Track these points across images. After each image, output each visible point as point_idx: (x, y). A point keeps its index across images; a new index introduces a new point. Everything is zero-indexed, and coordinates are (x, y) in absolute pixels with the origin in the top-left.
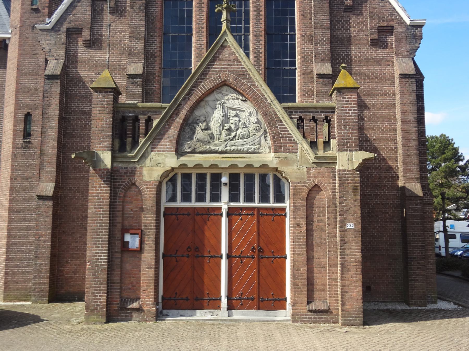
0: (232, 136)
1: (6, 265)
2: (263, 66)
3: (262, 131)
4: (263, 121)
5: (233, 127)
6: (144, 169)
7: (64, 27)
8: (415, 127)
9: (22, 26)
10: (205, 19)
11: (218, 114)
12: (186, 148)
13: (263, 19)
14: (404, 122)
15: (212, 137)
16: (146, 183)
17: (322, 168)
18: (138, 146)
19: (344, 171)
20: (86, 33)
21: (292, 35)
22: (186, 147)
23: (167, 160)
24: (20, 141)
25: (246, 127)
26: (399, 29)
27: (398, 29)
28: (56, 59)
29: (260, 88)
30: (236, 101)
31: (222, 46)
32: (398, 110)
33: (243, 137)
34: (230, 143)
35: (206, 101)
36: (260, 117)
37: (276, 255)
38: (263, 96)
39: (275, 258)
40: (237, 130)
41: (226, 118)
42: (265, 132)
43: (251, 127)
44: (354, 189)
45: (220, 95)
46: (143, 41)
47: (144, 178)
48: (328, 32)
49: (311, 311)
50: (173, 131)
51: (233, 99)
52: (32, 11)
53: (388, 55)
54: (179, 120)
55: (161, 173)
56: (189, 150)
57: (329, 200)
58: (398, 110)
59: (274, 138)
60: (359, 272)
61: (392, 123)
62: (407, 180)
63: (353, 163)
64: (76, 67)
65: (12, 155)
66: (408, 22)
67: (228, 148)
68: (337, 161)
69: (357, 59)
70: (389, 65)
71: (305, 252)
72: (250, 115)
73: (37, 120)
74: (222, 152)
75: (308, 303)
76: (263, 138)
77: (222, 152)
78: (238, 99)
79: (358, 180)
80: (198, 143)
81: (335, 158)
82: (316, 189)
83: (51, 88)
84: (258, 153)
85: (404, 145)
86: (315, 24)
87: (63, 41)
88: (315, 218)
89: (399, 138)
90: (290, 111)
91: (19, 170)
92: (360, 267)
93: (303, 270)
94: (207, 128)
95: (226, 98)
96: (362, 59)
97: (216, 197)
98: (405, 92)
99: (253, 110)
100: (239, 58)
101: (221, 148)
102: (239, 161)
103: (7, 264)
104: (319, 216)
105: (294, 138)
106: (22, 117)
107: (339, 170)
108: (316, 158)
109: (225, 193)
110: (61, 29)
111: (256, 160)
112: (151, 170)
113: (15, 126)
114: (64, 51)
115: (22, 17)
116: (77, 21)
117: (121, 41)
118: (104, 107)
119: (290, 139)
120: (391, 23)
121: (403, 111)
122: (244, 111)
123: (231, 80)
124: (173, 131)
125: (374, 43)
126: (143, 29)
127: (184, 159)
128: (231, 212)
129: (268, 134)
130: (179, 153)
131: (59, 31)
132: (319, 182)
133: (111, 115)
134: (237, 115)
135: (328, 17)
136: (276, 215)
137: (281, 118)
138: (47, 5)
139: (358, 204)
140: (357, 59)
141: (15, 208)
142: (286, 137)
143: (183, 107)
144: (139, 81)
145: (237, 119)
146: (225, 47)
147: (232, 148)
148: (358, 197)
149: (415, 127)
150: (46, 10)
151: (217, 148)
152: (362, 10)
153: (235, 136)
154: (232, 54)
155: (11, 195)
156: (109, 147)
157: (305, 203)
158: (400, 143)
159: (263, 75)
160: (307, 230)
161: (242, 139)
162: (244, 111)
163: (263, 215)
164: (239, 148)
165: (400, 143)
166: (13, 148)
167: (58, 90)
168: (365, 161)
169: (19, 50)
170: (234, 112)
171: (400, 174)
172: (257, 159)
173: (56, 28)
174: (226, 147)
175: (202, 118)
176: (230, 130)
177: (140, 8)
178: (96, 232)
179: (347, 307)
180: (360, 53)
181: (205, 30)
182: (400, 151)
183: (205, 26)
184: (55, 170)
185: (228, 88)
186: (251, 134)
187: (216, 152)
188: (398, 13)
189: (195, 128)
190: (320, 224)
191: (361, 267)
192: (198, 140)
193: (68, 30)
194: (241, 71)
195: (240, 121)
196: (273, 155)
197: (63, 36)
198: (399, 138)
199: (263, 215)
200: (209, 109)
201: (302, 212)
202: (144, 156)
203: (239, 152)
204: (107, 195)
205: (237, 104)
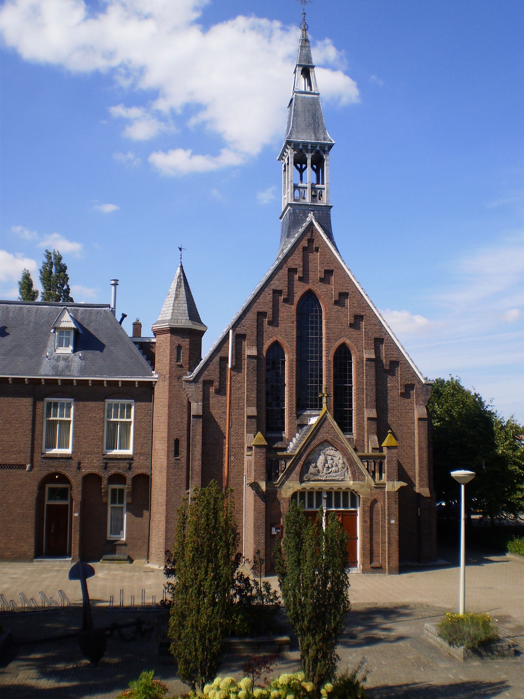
0: (330, 471)
1: (165, 543)
2: (332, 409)
3: (346, 468)
4: (346, 462)
5: (330, 466)
6: (282, 491)
7: (201, 380)
8: (426, 452)
9: (170, 377)
10: (295, 375)
11: (322, 458)
12: (305, 478)
13: (332, 377)
14: (420, 449)
15: (319, 471)
16: (284, 498)
17: (378, 490)
18: (278, 477)
19: (390, 492)
20: (216, 384)
21: (350, 386)
22: (305, 477)
23: (295, 486)
24: (173, 459)
25: (337, 466)
26: (419, 387)
27: (417, 386)
28: (196, 402)
29: (345, 444)
30: (332, 451)
31: (324, 419)
32: (416, 440)
33: (336, 472)
34: (328, 475)
35: (315, 451)
36: (345, 460)
37: (352, 538)
38: (347, 449)
39: (352, 539)
40: (332, 467)
41: (326, 461)
42: (348, 469)
43: (340, 466)
44: (395, 502)
45: (323, 447)
46: (255, 391)
47: (282, 496)
48: (374, 388)
49: (372, 568)
50: (298, 468)
51: (330, 450)
52: (177, 366)
53: (411, 403)
54: (301, 462)
55: (292, 493)
56: (306, 480)
57: (382, 508)
58: (416, 440)
59: (353, 473)
60: (397, 546)
61: (413, 448)
62: (421, 486)
63: (395, 488)
64: (209, 407)
65: (167, 468)
66: (424, 381)
67: (328, 478)
68: (386, 486)
69: (392, 405)
70: (411, 409)
71: (369, 536)
72: (339, 459)
73: (183, 444)
74: (325, 481)
75: (370, 563)
76: (346, 472)
77: (325, 481)
78: (332, 450)
79: (397, 497)
80: (311, 476)
81: (385, 484)
82: (375, 501)
83: (196, 424)
84: (344, 481)
85: (419, 464)
86: (366, 382)
87: (201, 389)
88: (374, 517)
89: (417, 458)
90: (362, 458)
91: (172, 479)
92: (398, 543)
93: (368, 545)
94: (316, 467)
95: (326, 449)
96: (395, 405)
97: (319, 504)
98: (421, 429)
99: (341, 456)
100: (333, 426)
101: (323, 478)
102: (334, 486)
103: (166, 543)
104: (376, 516)
105: (364, 473)
106: (173, 442)
107: (388, 492)
108: (376, 484)
109: (324, 503)
110: (199, 380)
111: (343, 485)
112: (286, 491)
113: (168, 448)
114: (202, 397)
115: (170, 370)
116: (210, 375)
117: (239, 389)
118: (260, 456)
119: (362, 474)
120: (413, 382)
121: (419, 442)
122: (336, 457)
123: (329, 439)
124: (298, 468)
125: (402, 395)
126: (255, 383)
127: (303, 485)
128: (328, 513)
129: (349, 470)
130: (302, 481)
131: (198, 382)
132: (377, 497)
133: (265, 461)
134: (332, 459)
135: (375, 378)
136: (352, 515)
137: (356, 461)
138: (188, 362)
139: (397, 510)
140: (392, 405)
141: (171, 505)
142: (360, 472)
143: (303, 455)
144: (254, 420)
145: (332, 461)
146: (326, 420)
147: (330, 478)
148: (397, 506)
149: (426, 452)
150: (187, 366)
151: (322, 478)
152: (395, 372)
153: (331, 472)
154: (329, 424)
155: (167, 495)
156: (264, 479)
157: (369, 509)
158: (417, 462)
159: (332, 415)
160: (370, 524)
161: (335, 473)
162: (336, 457)
163: (345, 515)
164: (334, 478)
165: (417, 462)
166: (167, 463)
167: (201, 425)
168: (402, 488)
169: (169, 394)
170: (330, 457)
171: (417, 484)
172: (344, 485)
173: (195, 380)
174: (327, 477)
175: (313, 461)
176: (328, 467)
177: (253, 368)
178: (258, 527)
179: (391, 565)
180: (393, 401)
181: (294, 383)
182: (417, 466)
183: (295, 380)
184: (200, 480)
185: (328, 444)
186: (340, 470)
187: (321, 480)
188: (417, 375)
189: (309, 467)
190: (377, 521)
191: (398, 543)
192: (311, 474)
193: (204, 381)
194: (335, 434)
195: (333, 462)
196: (352, 482)
197: (200, 385)
198: (417, 458)
199: (345, 515)
200: (317, 456)
201: (368, 514)
202: (283, 483)
203: (334, 480)
204: (264, 507)
205: (332, 452)
